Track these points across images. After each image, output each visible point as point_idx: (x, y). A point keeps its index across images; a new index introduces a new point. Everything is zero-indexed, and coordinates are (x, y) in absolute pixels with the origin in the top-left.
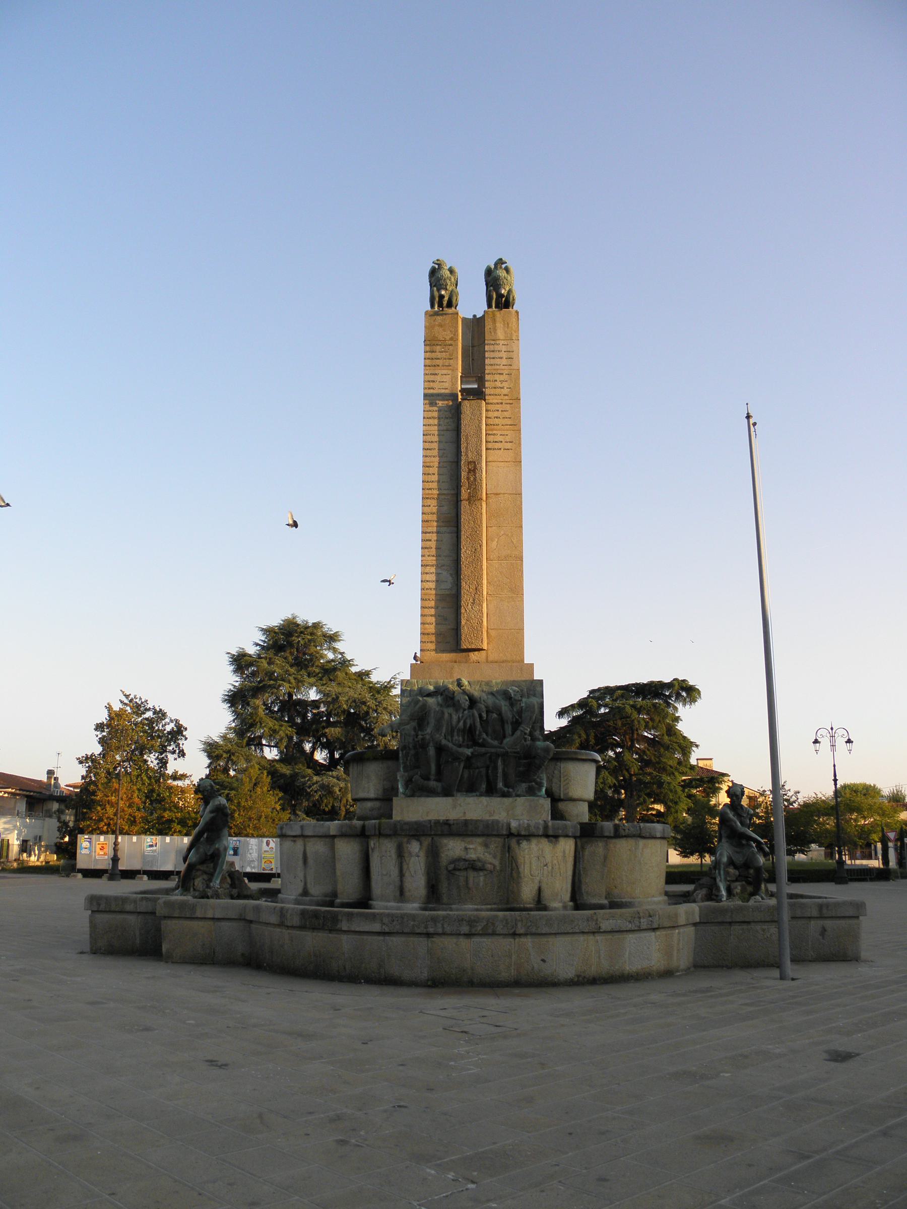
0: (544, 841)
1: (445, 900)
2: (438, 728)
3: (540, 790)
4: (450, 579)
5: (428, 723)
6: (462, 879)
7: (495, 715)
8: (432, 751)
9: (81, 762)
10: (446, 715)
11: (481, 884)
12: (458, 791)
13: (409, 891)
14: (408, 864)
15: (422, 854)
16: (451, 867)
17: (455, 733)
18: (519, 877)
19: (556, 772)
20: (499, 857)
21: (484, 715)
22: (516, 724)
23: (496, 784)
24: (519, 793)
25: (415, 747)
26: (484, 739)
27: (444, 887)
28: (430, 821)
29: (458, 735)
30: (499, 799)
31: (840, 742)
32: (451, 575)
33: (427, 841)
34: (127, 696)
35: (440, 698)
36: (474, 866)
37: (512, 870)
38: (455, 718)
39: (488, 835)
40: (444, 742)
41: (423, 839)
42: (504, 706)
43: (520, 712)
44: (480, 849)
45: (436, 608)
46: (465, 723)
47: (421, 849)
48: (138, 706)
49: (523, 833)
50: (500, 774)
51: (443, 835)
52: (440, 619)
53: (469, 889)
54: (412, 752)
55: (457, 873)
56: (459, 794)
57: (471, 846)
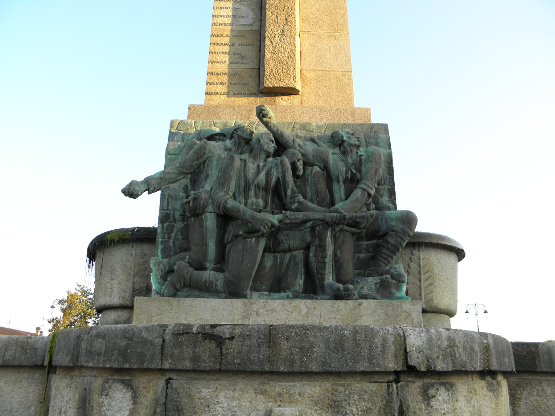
0: (480, 385)
2: (223, 182)
3: (399, 288)
4: (251, 15)
5: (207, 176)
7: (316, 169)
8: (210, 221)
9: (50, 322)
10: (237, 163)
12: (254, 289)
17: (252, 193)
19: (412, 265)
21: (300, 165)
22: (353, 182)
23: (322, 277)
24: (365, 291)
25: (184, 217)
26: (300, 203)
28: (164, 327)
29: (256, 196)
30: (330, 302)
31: (481, 312)
32: (253, 10)
33: (152, 388)
34: (79, 286)
35: (228, 143)
38: (252, 167)
39: (339, 374)
40: (231, 203)
41: (141, 381)
42: (333, 156)
43: (358, 165)
45: (232, 44)
46: (268, 174)
48: (85, 292)
49: (440, 366)
50: (329, 260)
51: (197, 372)
52: (236, 57)
54: (179, 225)
56: (255, 294)
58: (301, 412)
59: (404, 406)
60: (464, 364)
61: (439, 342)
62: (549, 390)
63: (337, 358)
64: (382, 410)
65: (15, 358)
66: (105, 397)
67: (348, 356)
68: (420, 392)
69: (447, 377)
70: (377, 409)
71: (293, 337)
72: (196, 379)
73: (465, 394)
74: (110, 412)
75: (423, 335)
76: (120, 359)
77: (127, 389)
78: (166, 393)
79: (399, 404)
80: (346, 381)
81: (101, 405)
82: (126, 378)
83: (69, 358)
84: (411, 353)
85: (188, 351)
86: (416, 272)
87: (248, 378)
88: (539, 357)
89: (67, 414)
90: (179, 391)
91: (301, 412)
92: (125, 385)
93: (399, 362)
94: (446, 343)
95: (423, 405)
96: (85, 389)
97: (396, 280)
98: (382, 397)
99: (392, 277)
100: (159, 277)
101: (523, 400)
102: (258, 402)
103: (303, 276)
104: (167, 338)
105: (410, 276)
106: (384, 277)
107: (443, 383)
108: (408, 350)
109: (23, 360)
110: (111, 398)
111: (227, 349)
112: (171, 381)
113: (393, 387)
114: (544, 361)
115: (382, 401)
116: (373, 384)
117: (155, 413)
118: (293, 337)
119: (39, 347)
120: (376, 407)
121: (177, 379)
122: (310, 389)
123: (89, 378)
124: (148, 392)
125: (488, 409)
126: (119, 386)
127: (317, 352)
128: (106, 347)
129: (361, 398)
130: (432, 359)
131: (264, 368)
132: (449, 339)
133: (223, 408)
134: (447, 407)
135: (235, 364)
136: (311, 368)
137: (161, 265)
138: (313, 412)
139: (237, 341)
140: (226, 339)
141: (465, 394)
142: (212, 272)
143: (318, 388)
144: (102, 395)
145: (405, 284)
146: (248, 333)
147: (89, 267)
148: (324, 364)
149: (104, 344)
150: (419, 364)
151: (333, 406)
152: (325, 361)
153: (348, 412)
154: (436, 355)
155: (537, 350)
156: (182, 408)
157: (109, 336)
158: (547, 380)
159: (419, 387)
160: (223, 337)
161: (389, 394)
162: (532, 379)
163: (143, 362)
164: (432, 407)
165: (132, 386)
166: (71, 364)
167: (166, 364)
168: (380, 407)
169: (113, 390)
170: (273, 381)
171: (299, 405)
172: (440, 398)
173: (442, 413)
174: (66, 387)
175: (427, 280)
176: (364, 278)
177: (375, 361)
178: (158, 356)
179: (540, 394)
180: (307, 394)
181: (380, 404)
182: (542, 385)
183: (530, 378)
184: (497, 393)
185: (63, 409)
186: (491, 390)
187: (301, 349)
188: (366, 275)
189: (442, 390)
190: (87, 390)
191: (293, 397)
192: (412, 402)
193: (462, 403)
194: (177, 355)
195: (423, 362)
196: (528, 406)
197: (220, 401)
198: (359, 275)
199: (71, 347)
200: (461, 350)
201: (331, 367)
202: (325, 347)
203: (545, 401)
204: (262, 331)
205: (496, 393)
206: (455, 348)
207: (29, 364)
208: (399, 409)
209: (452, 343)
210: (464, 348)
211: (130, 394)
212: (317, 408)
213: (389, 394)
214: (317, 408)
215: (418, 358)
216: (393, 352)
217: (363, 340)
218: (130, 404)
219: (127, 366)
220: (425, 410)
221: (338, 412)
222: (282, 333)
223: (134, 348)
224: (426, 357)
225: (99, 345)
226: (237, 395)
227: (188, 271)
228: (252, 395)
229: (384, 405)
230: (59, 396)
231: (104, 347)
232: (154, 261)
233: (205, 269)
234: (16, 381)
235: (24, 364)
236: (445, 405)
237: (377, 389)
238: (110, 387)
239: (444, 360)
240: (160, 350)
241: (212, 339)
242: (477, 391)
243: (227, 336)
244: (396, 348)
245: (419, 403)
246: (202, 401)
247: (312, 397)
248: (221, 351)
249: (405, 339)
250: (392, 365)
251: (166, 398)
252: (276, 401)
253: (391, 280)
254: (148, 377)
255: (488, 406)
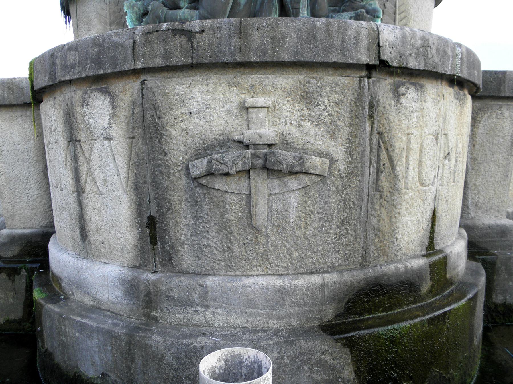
1: (186, 259)
6: (234, 205)
11: (292, 215)
13: (98, 230)
14: (88, 161)
15: (118, 131)
16: (199, 167)
18: (395, 190)
20: (344, 131)
27: (180, 226)
33: (128, 91)
36: (268, 162)
37: (379, 171)
44: (289, 110)
47: (113, 116)
49: (413, 64)
51: (170, 69)
53: (257, 230)
55: (219, 184)
57: (260, 101)
58: (274, 103)
59: (374, 100)
60: (436, 66)
61: (412, 40)
62: (507, 113)
63: (310, 48)
64: (353, 103)
65: (4, 98)
66: (86, 107)
67: (320, 47)
68: (391, 89)
69: (418, 79)
70: (348, 101)
71: (264, 27)
72: (170, 78)
73: (433, 96)
74: (93, 120)
75: (397, 31)
76: (94, 66)
77: (105, 96)
78: (142, 94)
79: (370, 98)
80: (318, 74)
81: (83, 115)
82: (103, 86)
83: (47, 78)
84: (384, 47)
85: (159, 49)
86: (391, 11)
87: (220, 73)
88: (504, 83)
89: (57, 130)
90: (154, 90)
91: (274, 103)
92: (103, 93)
93: (371, 56)
94: (420, 42)
95: (393, 102)
96: (68, 104)
97: (371, 15)
98: (354, 90)
99: (367, 12)
100: (134, 20)
101: (482, 122)
102: (231, 95)
103: (278, 12)
104: (137, 38)
105: (385, 15)
106: (359, 11)
107: (414, 83)
108: (381, 44)
109: (11, 99)
110: (91, 107)
111: (198, 42)
112: (146, 82)
113: (365, 82)
114: (508, 86)
115: (353, 94)
116: (345, 78)
117: (133, 113)
118: (264, 27)
119: (25, 86)
120: (347, 99)
121: (151, 80)
122: (283, 81)
123: (69, 94)
124: (125, 95)
125: (453, 115)
126: (98, 94)
127: (289, 42)
128: (79, 58)
129: (332, 90)
130: (404, 56)
131: (236, 60)
132: (423, 38)
133: (197, 102)
134: (415, 105)
135: (207, 56)
136: (283, 58)
137: (135, 8)
138: (286, 102)
139: (208, 34)
140: (196, 32)
141: (433, 96)
142: (187, 10)
143: (290, 79)
144: (83, 106)
145: (380, 19)
146: (218, 25)
147: (66, 24)
148: (296, 54)
149: (77, 55)
150: (391, 59)
151: (305, 97)
152: (297, 51)
153: (320, 103)
154: (409, 52)
155: (504, 76)
156: (158, 106)
157: (80, 47)
158: (508, 105)
159: (390, 84)
160: (193, 31)
161: (361, 88)
162: (494, 104)
163: (116, 65)
164: (401, 104)
165: (109, 92)
166: (51, 83)
167: (139, 64)
168: (352, 100)
169: (93, 99)
170: (245, 74)
171: (272, 96)
172: (410, 97)
173: (411, 111)
174: (51, 108)
175: (401, 20)
176: (339, 13)
177: (347, 53)
178: (130, 57)
179: (499, 117)
180: (279, 86)
181: (351, 97)
182: (502, 109)
183: (493, 103)
184: (463, 103)
185: (53, 128)
186: (457, 99)
187: (273, 39)
188: (341, 11)
189: (412, 89)
190: (69, 105)
191: (266, 89)
192: (382, 97)
193: (429, 104)
194: (148, 53)
195: (396, 57)
196: (486, 127)
197: (194, 96)
198: (333, 11)
199: (48, 67)
200: (434, 51)
201: (304, 57)
202: (297, 37)
203: (502, 122)
204: (232, 23)
205: (461, 103)
206: (429, 49)
207: (19, 103)
208: (369, 103)
209: (426, 44)
210: (437, 50)
211: (109, 100)
212: (289, 99)
213: (361, 88)
214: (289, 99)
215: (391, 53)
216: (366, 46)
217: (335, 31)
218: (109, 109)
219: (101, 72)
220: (394, 106)
221: (310, 102)
222: (253, 24)
223: (106, 53)
224: (399, 52)
225: (72, 58)
226: (210, 89)
227: (163, 11)
228: (225, 88)
229: (355, 98)
230: (47, 118)
231: (77, 58)
232: (128, 4)
233: (180, 8)
234: (11, 119)
235: (14, 103)
236: (414, 104)
237: (349, 83)
238: (89, 97)
239: (416, 58)
240: (132, 51)
241: (182, 35)
242: (445, 96)
243: (197, 30)
244: (370, 42)
245: (389, 99)
246: (177, 97)
247: (285, 88)
248: (192, 44)
249: (379, 34)
250: (364, 59)
251: (143, 98)
252: (249, 92)
253: (365, 14)
254: (123, 82)
255: (453, 111)
